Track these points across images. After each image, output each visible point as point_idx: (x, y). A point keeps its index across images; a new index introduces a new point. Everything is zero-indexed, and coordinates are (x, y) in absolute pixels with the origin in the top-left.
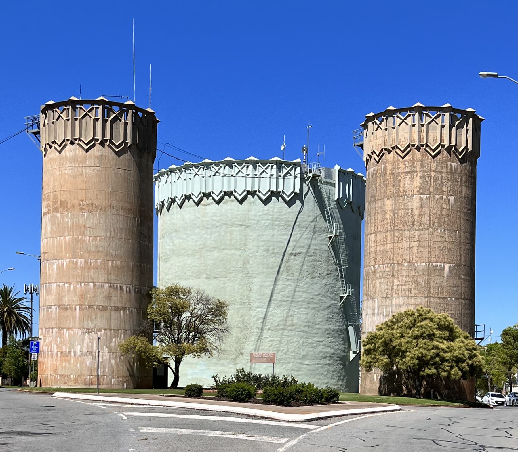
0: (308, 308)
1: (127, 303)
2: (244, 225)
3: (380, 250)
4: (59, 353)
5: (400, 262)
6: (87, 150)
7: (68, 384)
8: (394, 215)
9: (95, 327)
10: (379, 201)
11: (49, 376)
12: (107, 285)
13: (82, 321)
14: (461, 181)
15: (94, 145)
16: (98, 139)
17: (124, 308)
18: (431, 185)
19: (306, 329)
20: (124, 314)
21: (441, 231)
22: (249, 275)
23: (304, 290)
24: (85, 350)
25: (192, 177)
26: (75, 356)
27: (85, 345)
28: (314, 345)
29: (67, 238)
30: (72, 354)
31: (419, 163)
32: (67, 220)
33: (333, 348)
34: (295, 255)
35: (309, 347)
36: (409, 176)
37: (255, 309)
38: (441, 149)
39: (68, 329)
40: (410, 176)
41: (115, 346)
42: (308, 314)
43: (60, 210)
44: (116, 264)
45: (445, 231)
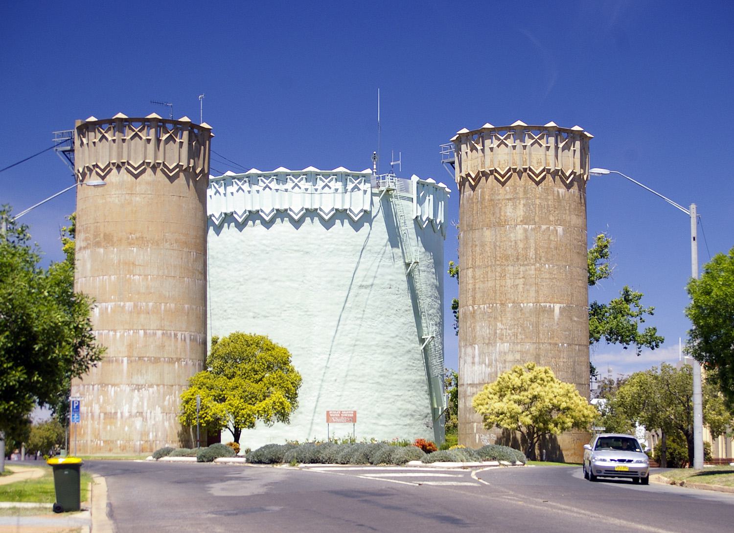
0: (383, 353)
1: (182, 354)
2: (302, 251)
3: (479, 288)
4: (102, 415)
5: (503, 302)
6: (136, 176)
7: (114, 451)
8: (495, 248)
9: (146, 383)
10: (477, 231)
11: (89, 442)
12: (159, 333)
13: (130, 375)
14: (569, 208)
15: (144, 171)
16: (150, 163)
17: (179, 360)
18: (536, 213)
19: (381, 380)
20: (179, 367)
21: (549, 266)
22: (308, 313)
23: (377, 331)
24: (134, 411)
25: (235, 192)
26: (122, 417)
27: (134, 405)
28: (391, 400)
29: (113, 277)
30: (119, 415)
31: (522, 190)
32: (112, 256)
33: (414, 404)
34: (366, 287)
35: (385, 404)
36: (510, 203)
37: (317, 355)
38: (545, 175)
39: (112, 385)
40: (512, 204)
41: (169, 404)
42: (383, 361)
43: (103, 244)
44: (170, 307)
45: (553, 267)
